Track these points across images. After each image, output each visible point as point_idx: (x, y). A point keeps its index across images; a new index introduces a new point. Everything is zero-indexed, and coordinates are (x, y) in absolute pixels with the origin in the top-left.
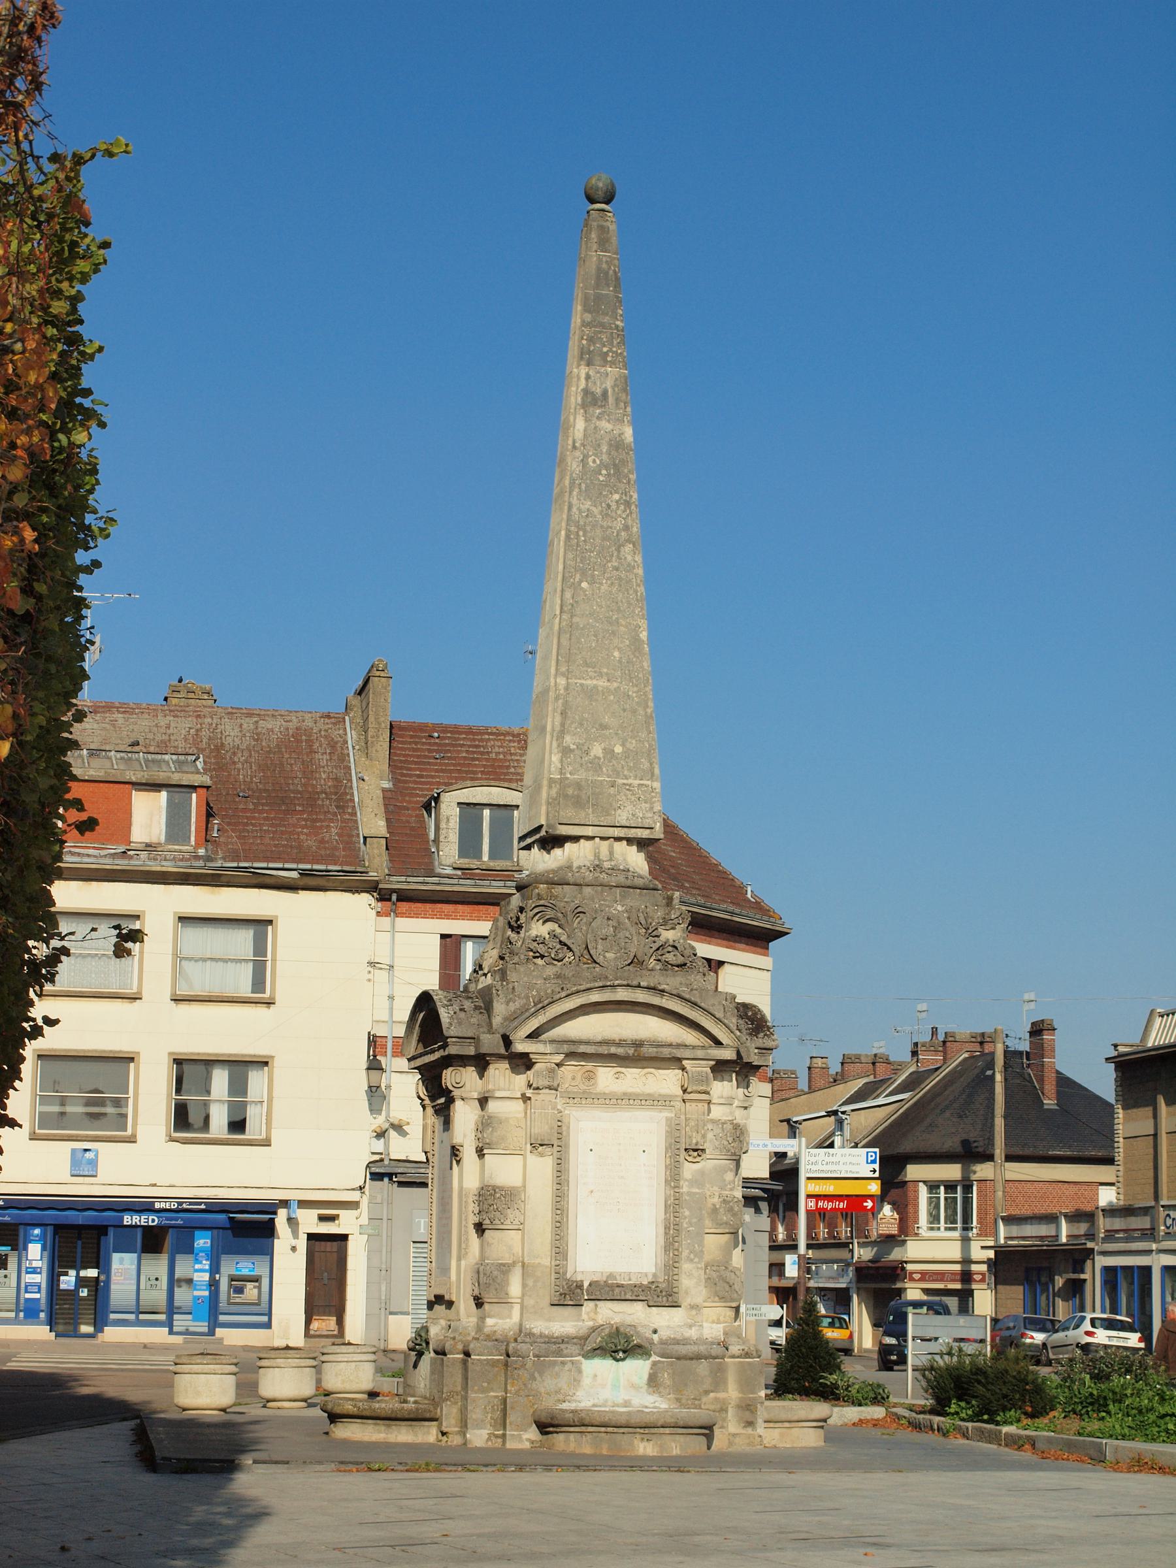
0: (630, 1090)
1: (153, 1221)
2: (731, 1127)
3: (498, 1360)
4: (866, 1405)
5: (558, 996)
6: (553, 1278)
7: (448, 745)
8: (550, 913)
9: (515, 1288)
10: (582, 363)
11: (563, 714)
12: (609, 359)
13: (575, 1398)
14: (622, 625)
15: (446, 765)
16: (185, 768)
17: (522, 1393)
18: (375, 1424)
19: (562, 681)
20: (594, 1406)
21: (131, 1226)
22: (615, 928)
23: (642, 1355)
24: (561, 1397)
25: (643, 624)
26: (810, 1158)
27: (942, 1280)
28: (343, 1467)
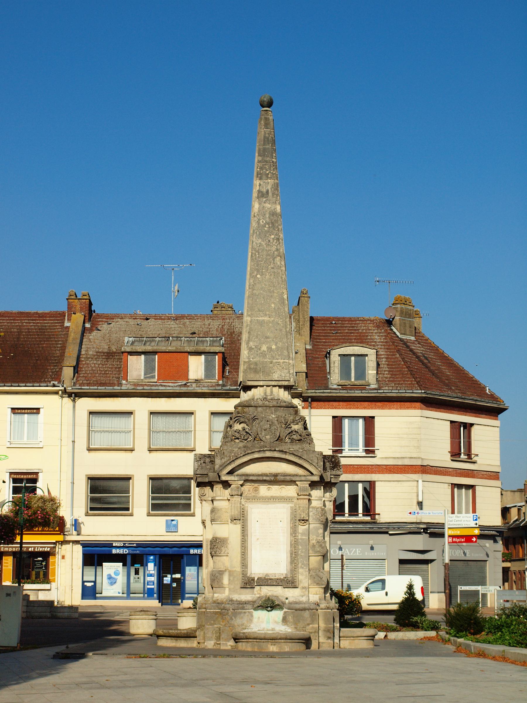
0: (274, 495)
1: (126, 551)
2: (320, 510)
3: (218, 612)
4: (429, 630)
5: (239, 456)
6: (241, 576)
7: (339, 327)
8: (242, 420)
9: (226, 580)
10: (258, 179)
14: (275, 293)
15: (338, 336)
16: (215, 344)
17: (227, 625)
18: (171, 639)
20: (259, 630)
21: (193, 554)
22: (270, 425)
23: (279, 609)
24: (244, 627)
25: (285, 291)
28: (129, 656)
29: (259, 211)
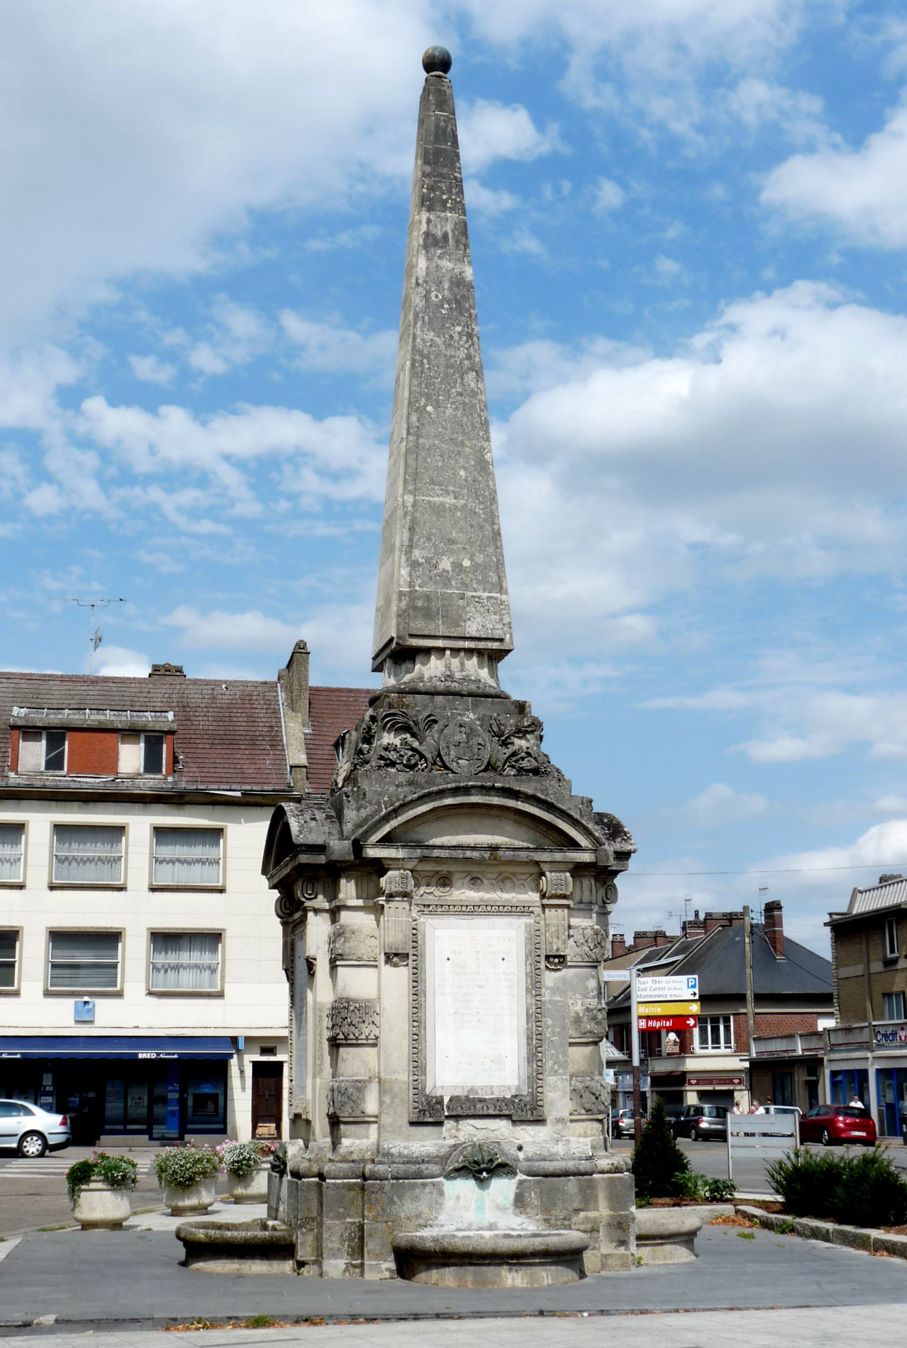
2: (591, 932)
3: (355, 1184)
10: (423, 209)
11: (411, 529)
12: (449, 205)
13: (437, 1222)
14: (467, 446)
19: (410, 499)
20: (458, 1230)
24: (422, 1222)
26: (639, 986)
27: (711, 1084)
29: (428, 274)
